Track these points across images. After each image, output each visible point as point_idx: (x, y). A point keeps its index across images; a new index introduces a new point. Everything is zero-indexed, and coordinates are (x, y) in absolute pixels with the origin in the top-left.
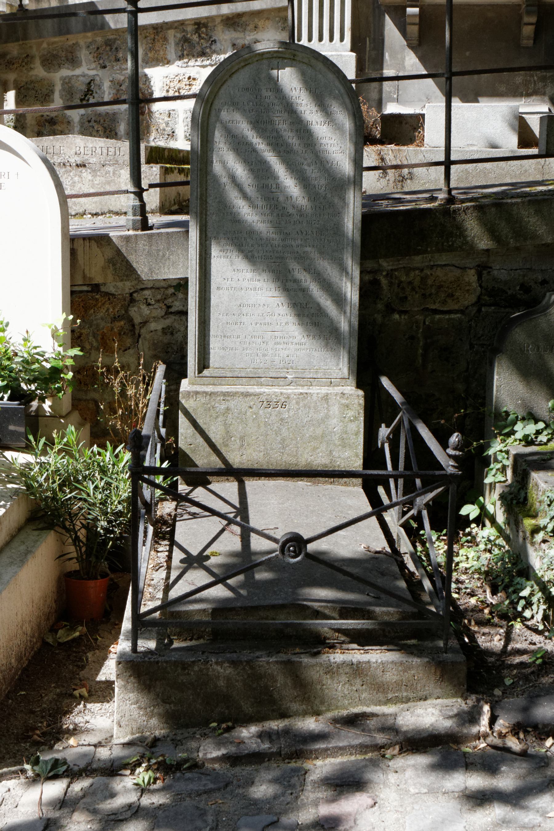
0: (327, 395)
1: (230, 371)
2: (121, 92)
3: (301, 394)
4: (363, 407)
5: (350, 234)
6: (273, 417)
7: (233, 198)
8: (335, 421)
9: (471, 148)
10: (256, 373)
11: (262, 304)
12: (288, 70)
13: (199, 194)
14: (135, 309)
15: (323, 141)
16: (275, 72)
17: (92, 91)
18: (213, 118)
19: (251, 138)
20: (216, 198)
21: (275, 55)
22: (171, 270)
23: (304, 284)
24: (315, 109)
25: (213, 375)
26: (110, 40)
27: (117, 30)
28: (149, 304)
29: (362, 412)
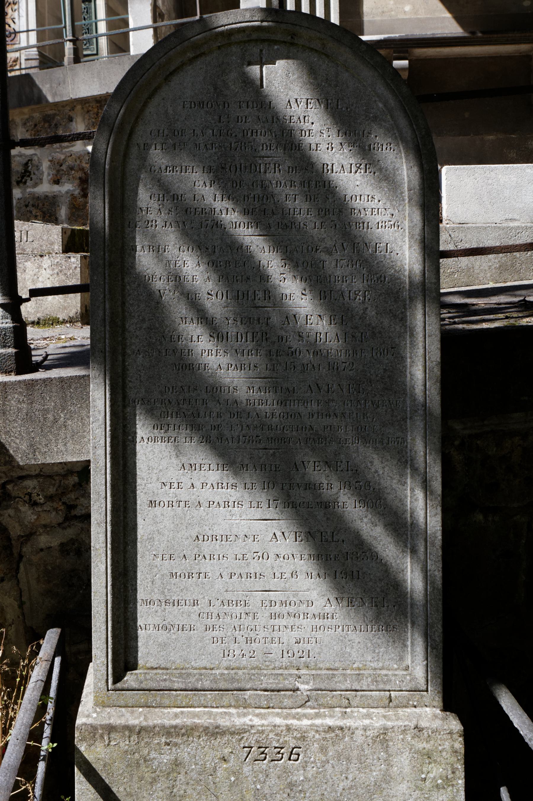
0: (385, 731)
1: (181, 675)
2: (61, 172)
3: (330, 729)
4: (461, 757)
5: (419, 390)
6: (273, 781)
7: (178, 320)
8: (403, 787)
9: (512, 224)
10: (233, 680)
11: (242, 536)
12: (280, 63)
13: (107, 312)
14: (11, 512)
15: (357, 204)
16: (255, 69)
17: (30, 172)
18: (133, 163)
19: (211, 199)
20: (143, 320)
21: (254, 36)
22: (70, 446)
23: (327, 493)
24: (336, 141)
25: (143, 686)
26: (49, 116)
27: (56, 104)
28: (34, 504)
29: (460, 767)
